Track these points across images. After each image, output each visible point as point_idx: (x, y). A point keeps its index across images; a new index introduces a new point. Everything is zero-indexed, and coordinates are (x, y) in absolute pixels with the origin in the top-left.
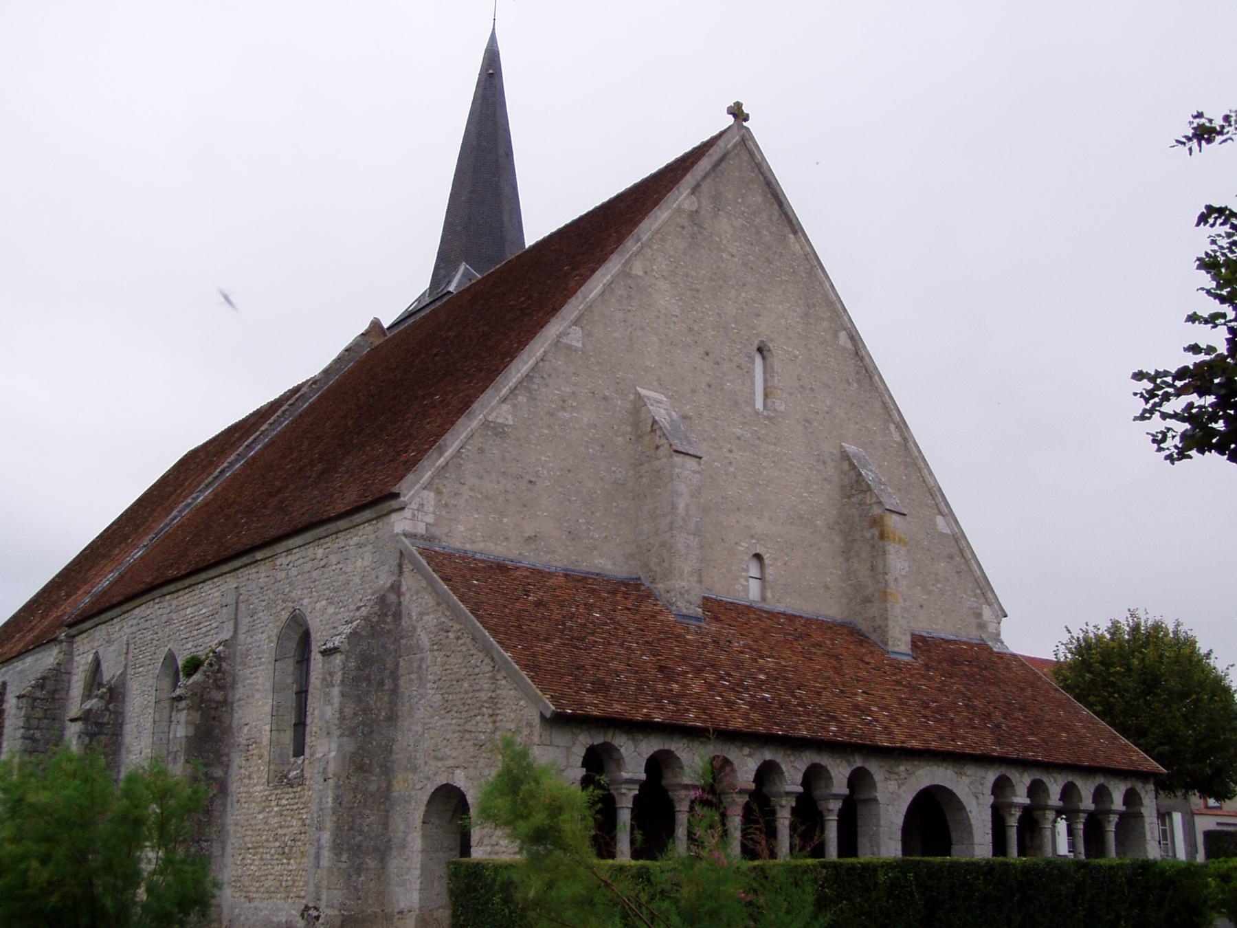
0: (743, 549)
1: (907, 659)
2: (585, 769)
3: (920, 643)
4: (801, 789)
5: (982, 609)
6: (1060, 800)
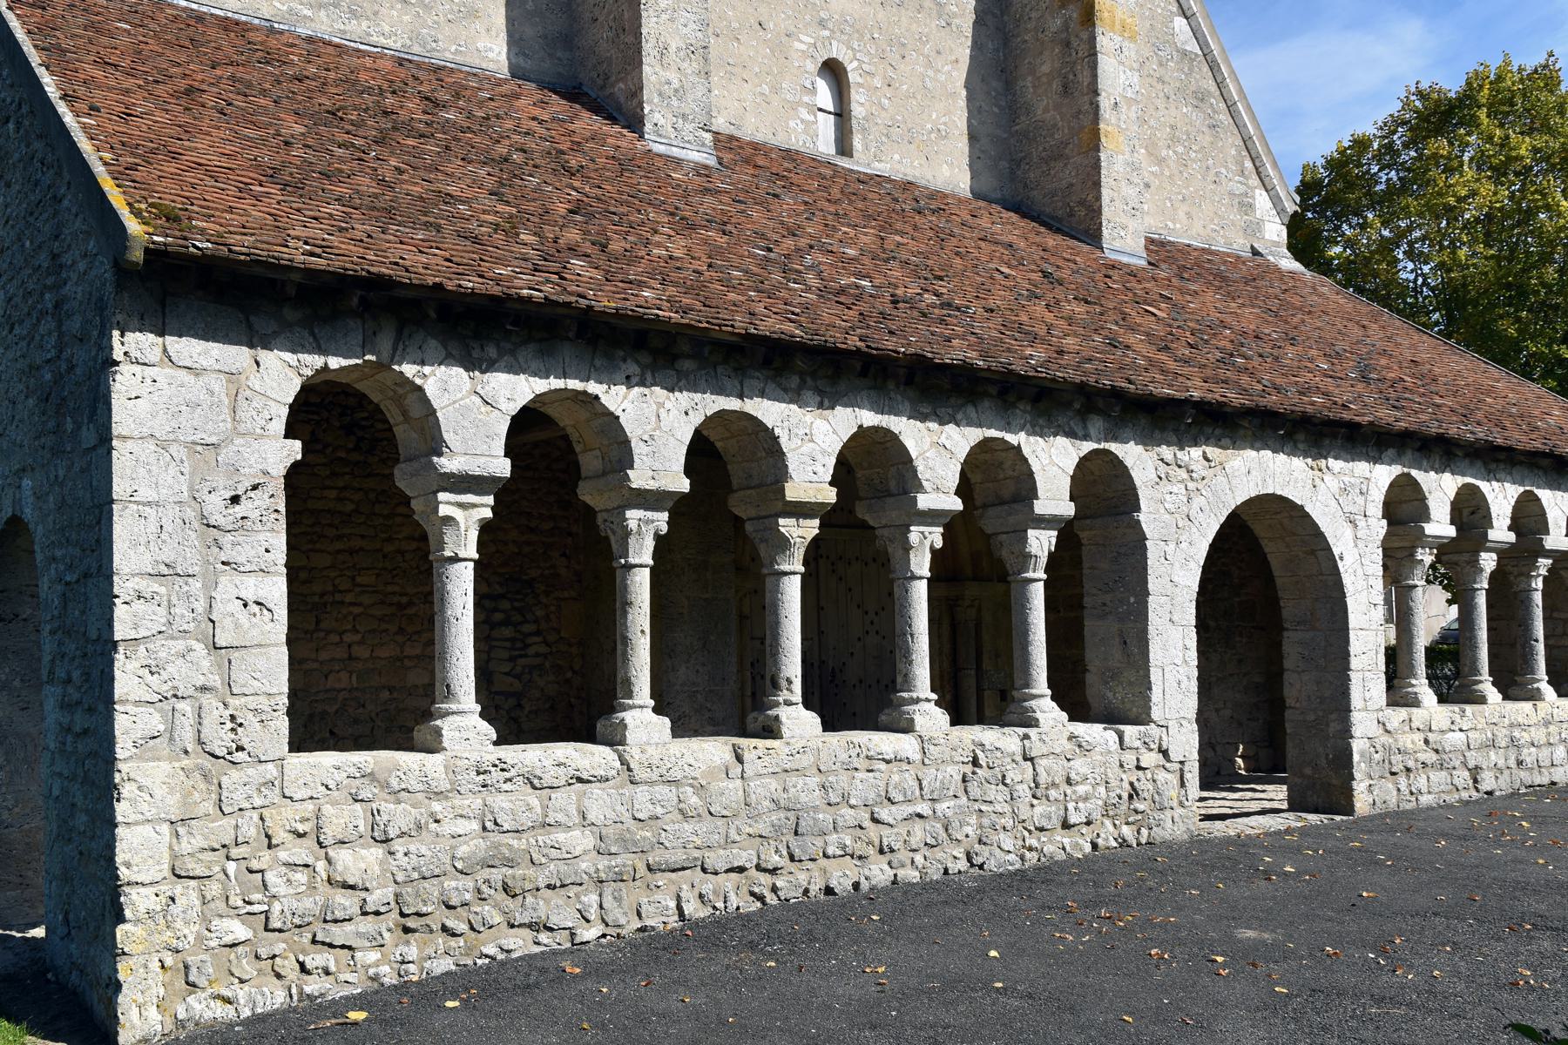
0: (803, 47)
1: (1143, 263)
2: (298, 444)
3: (1158, 248)
4: (957, 504)
5: (1253, 197)
6: (1510, 529)
